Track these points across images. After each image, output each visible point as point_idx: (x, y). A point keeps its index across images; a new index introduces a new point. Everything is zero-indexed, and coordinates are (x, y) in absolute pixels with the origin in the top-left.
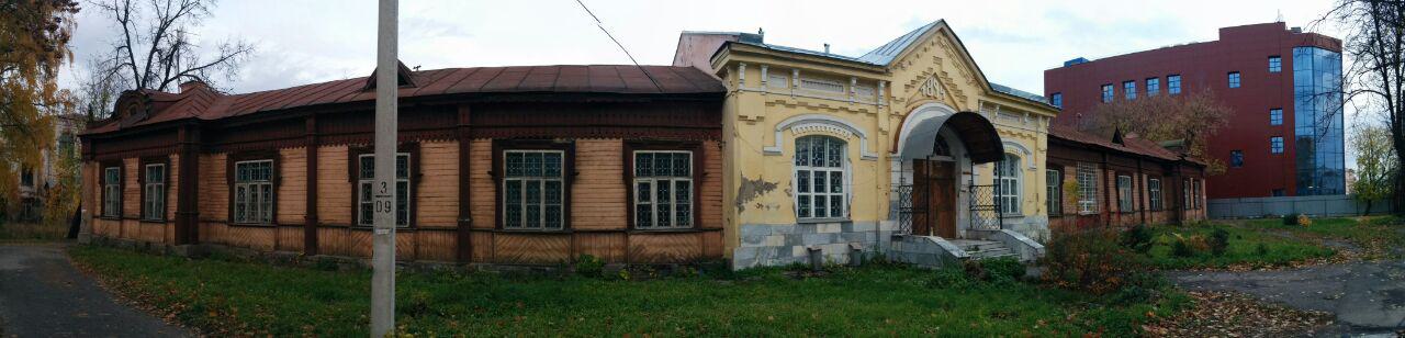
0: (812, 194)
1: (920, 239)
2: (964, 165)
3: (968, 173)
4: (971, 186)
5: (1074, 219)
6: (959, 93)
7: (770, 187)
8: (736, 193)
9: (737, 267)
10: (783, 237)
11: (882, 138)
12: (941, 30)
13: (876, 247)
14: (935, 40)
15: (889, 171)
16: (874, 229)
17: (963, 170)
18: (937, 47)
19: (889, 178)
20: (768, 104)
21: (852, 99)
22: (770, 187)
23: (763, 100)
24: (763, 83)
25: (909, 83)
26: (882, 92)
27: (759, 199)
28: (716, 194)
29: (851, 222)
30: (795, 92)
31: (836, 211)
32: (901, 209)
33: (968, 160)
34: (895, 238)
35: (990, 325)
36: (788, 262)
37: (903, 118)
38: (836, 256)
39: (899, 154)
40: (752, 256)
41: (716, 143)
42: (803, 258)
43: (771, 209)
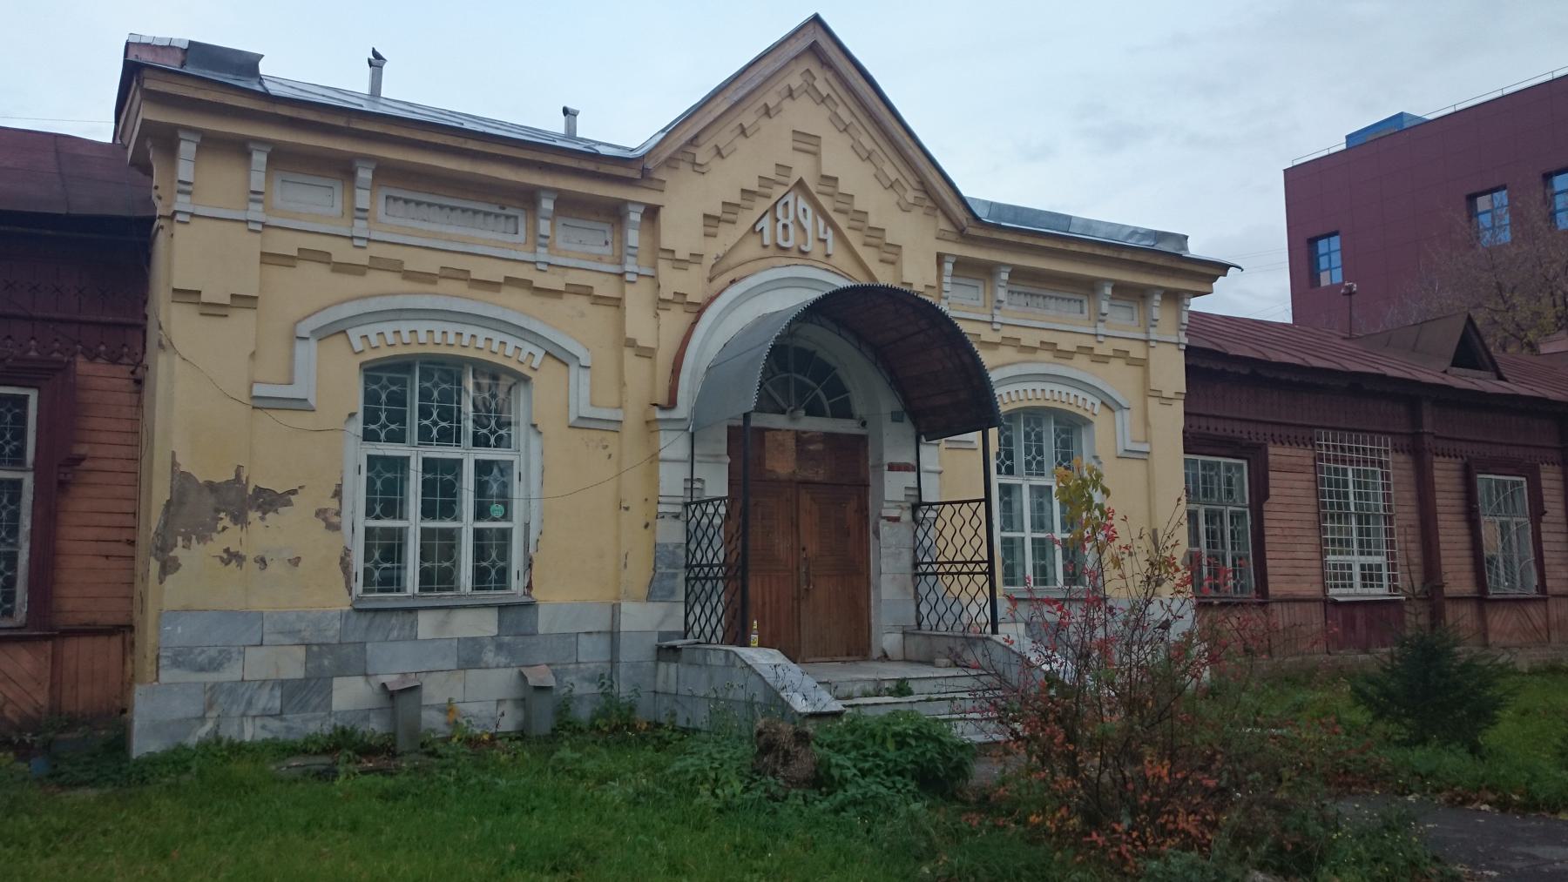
0: (413, 523)
1: (717, 653)
2: (894, 443)
3: (904, 467)
4: (917, 505)
5: (1315, 619)
6: (875, 236)
7: (269, 501)
8: (156, 518)
9: (143, 745)
10: (300, 652)
11: (635, 368)
12: (814, 50)
13: (605, 680)
14: (795, 80)
15: (654, 459)
16: (604, 625)
17: (889, 458)
18: (804, 103)
19: (653, 479)
20: (268, 258)
21: (543, 254)
22: (269, 501)
23: (254, 245)
24: (256, 196)
25: (717, 210)
26: (633, 237)
27: (229, 536)
28: (118, 520)
29: (531, 605)
30: (360, 228)
31: (490, 574)
32: (688, 567)
33: (907, 428)
34: (667, 652)
35: (388, 829)
36: (313, 728)
37: (699, 310)
38: (473, 708)
39: (683, 410)
40: (194, 709)
41: (123, 371)
42: (365, 715)
43: (273, 567)
